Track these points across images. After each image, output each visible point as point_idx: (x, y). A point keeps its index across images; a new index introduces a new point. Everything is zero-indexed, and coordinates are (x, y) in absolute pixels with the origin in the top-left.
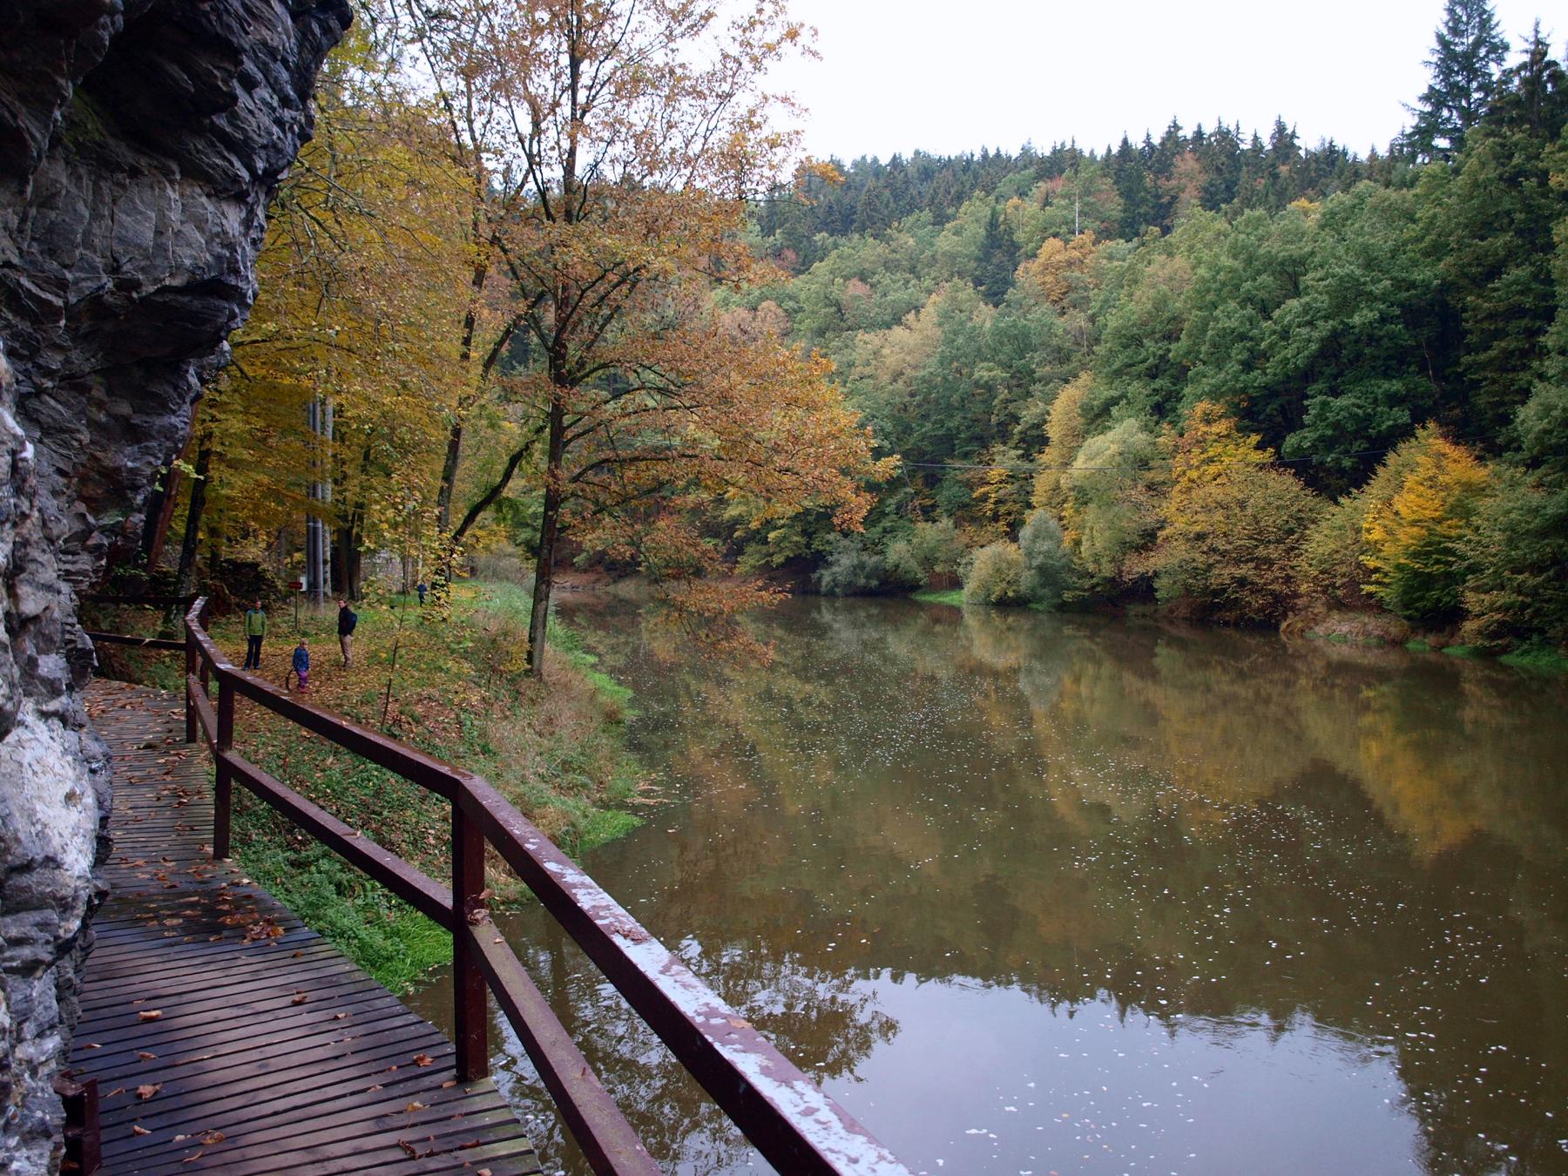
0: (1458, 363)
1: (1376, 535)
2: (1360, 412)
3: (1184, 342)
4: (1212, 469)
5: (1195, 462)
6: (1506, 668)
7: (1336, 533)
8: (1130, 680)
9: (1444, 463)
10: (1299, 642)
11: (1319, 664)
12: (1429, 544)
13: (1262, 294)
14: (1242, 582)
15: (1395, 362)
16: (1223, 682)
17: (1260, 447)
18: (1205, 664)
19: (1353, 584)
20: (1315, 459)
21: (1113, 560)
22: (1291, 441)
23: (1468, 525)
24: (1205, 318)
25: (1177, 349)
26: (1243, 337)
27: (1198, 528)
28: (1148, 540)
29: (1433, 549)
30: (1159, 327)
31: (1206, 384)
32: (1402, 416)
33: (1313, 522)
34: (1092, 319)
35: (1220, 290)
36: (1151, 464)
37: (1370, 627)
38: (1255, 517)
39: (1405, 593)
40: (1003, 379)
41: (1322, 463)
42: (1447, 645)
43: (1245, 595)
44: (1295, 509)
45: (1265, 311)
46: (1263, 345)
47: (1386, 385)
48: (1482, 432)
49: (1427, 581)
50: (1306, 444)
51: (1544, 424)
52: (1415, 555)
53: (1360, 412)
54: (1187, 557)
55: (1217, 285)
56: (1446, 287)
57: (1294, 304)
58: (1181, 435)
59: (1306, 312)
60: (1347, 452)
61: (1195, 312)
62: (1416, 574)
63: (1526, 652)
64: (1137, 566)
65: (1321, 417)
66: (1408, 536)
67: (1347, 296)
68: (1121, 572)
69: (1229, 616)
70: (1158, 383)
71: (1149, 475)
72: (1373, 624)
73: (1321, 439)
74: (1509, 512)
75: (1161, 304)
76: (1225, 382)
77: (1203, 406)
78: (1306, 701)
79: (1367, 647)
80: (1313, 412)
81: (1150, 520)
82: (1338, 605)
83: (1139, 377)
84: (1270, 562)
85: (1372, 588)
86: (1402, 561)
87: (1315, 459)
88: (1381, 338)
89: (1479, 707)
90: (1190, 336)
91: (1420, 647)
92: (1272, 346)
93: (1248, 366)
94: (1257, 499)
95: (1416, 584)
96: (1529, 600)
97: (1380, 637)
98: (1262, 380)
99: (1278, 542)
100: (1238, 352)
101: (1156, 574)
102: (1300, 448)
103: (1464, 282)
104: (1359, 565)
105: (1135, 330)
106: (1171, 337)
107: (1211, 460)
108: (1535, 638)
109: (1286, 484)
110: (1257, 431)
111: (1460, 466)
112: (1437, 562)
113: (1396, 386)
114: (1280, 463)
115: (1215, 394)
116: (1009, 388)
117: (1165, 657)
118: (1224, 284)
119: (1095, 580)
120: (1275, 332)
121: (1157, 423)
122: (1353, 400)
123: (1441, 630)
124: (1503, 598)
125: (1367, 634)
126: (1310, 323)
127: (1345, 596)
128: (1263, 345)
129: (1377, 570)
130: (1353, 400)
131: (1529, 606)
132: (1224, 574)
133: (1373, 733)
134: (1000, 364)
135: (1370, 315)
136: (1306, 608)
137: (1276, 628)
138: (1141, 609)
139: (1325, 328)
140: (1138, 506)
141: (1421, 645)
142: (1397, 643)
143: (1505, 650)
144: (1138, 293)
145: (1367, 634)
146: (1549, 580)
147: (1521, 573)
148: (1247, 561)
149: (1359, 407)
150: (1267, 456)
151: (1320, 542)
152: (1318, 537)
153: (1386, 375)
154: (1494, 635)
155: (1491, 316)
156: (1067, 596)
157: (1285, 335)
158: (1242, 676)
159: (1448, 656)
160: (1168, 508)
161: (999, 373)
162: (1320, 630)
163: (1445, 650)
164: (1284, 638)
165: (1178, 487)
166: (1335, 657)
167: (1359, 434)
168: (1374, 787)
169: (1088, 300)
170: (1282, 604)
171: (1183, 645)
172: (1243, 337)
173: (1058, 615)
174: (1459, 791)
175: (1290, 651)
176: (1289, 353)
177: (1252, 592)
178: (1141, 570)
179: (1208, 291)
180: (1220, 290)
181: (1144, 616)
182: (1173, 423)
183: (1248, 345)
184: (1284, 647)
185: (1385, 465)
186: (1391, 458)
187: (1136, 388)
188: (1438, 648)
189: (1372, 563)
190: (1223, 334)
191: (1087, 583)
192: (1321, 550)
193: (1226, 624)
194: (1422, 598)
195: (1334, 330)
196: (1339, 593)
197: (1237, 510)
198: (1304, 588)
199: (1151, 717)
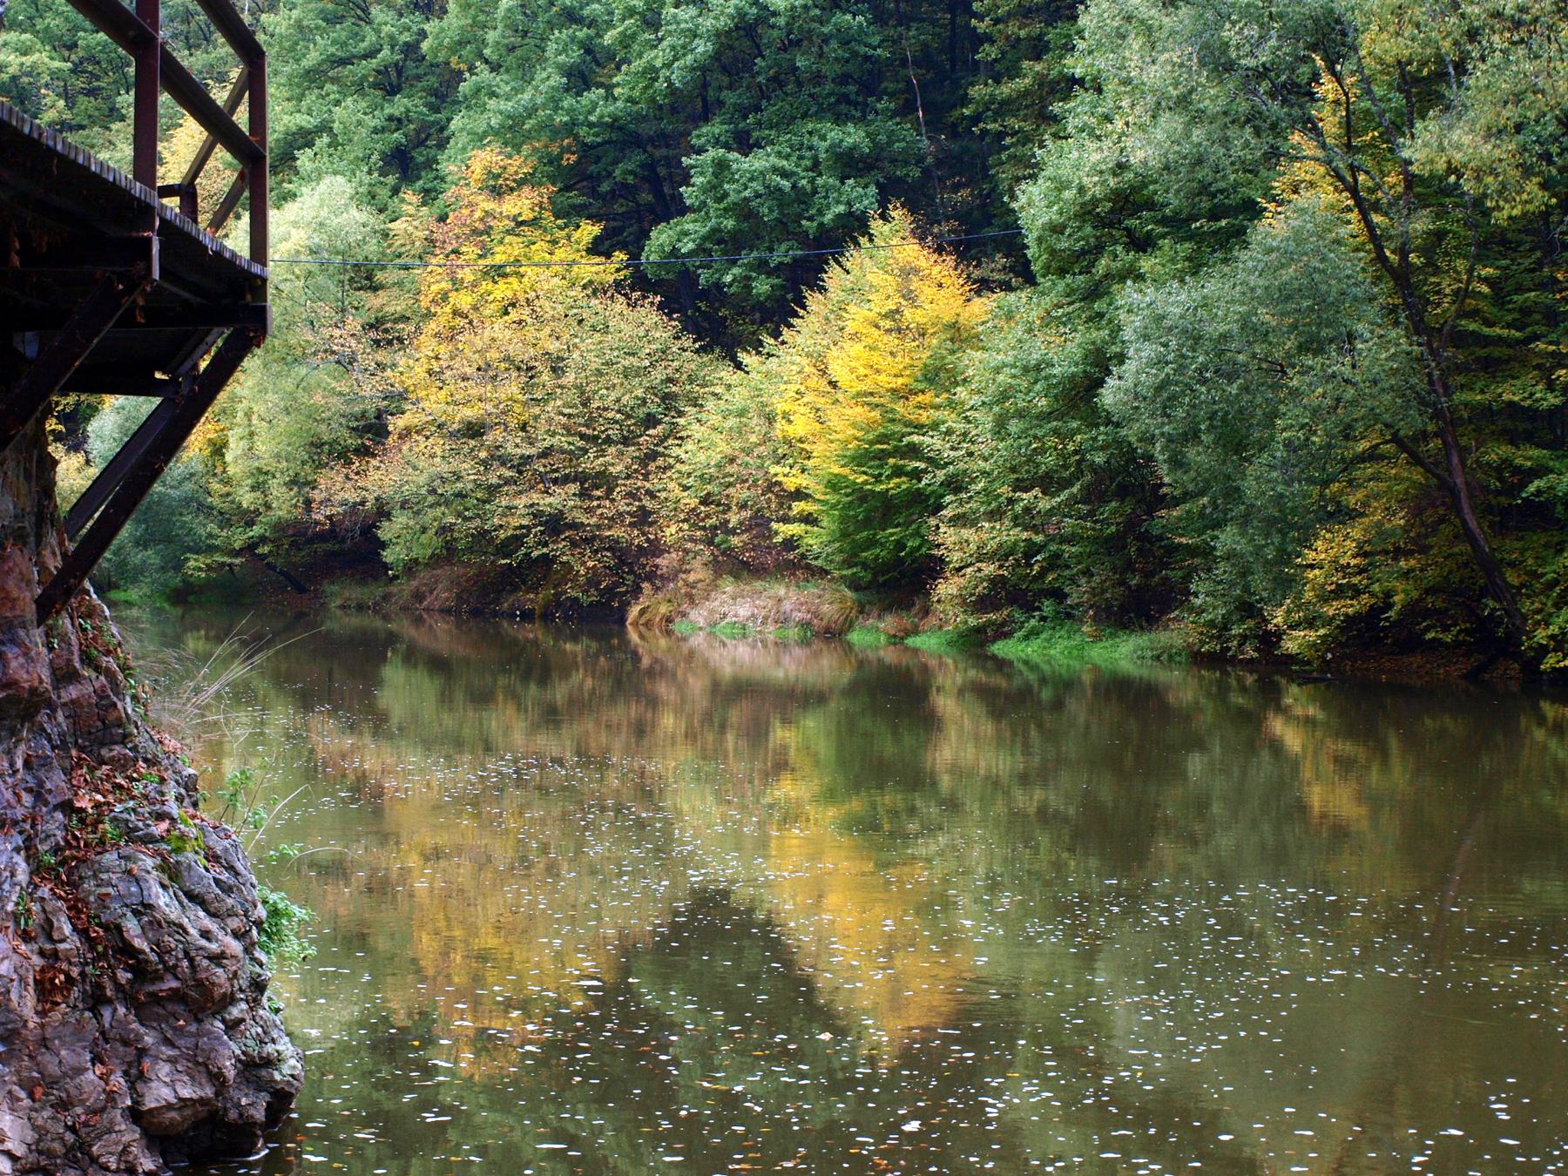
0: (965, 101)
1: (801, 426)
2: (786, 184)
4: (502, 290)
5: (467, 275)
6: (1001, 664)
7: (732, 422)
8: (328, 735)
9: (915, 284)
11: (697, 685)
12: (884, 438)
14: (554, 524)
15: (855, 91)
17: (598, 248)
18: (482, 698)
19: (759, 524)
21: (293, 482)
22: (661, 237)
23: (952, 405)
27: (469, 413)
28: (371, 433)
29: (887, 449)
31: (496, 111)
32: (861, 194)
37: (787, 606)
39: (844, 535)
40: (55, 75)
41: (718, 286)
42: (915, 631)
44: (658, 375)
46: (609, 38)
47: (834, 134)
48: (981, 239)
49: (883, 510)
50: (687, 246)
51: (1052, 215)
53: (786, 184)
54: (444, 468)
58: (442, 219)
60: (762, 266)
62: (862, 496)
63: (1034, 633)
64: (338, 491)
65: (714, 190)
68: (308, 503)
69: (534, 600)
70: (399, 105)
72: (793, 597)
73: (715, 236)
76: (532, 111)
77: (486, 158)
78: (672, 762)
79: (782, 645)
80: (698, 180)
81: (370, 391)
83: (359, 88)
84: (604, 480)
85: (795, 529)
87: (704, 277)
88: (826, 39)
92: (626, 41)
93: (579, 79)
94: (586, 352)
96: (1039, 539)
97: (805, 625)
98: (604, 111)
99: (626, 441)
100: (561, 48)
102: (674, 252)
104: (772, 485)
107: (498, 272)
108: (1048, 606)
109: (644, 325)
110: (594, 218)
111: (941, 291)
112: (898, 472)
113: (853, 136)
114: (638, 283)
115: (512, 133)
116: (69, 97)
117: (401, 688)
119: (257, 530)
121: (395, 191)
122: (774, 160)
123: (908, 607)
124: (1006, 534)
125: (783, 621)
127: (744, 549)
128: (609, 38)
129: (799, 495)
130: (774, 160)
132: (516, 509)
134: (48, 38)
137: (622, 620)
138: (355, 593)
140: (347, 363)
141: (872, 637)
142: (833, 634)
145: (783, 621)
147: (1026, 490)
149: (785, 174)
150: (608, 270)
151: (703, 443)
152: (697, 431)
153: (840, 119)
156: (196, 564)
158: (551, 717)
159: (916, 651)
160: (409, 368)
161: (44, 59)
162: (698, 616)
163: (910, 641)
164: (634, 636)
165: (432, 326)
166: (727, 671)
167: (786, 228)
168: (798, 928)
170: (632, 567)
171: (439, 665)
174: (934, 906)
175: (646, 662)
176: (658, 57)
177: (574, 544)
181: (361, 608)
183: (582, 33)
184: (636, 657)
185: (822, 290)
186: (834, 277)
187: (350, 112)
188: (897, 639)
191: (239, 538)
193: (527, 616)
194: (871, 543)
196: (735, 541)
197: (546, 377)
198: (671, 532)
199: (368, 803)
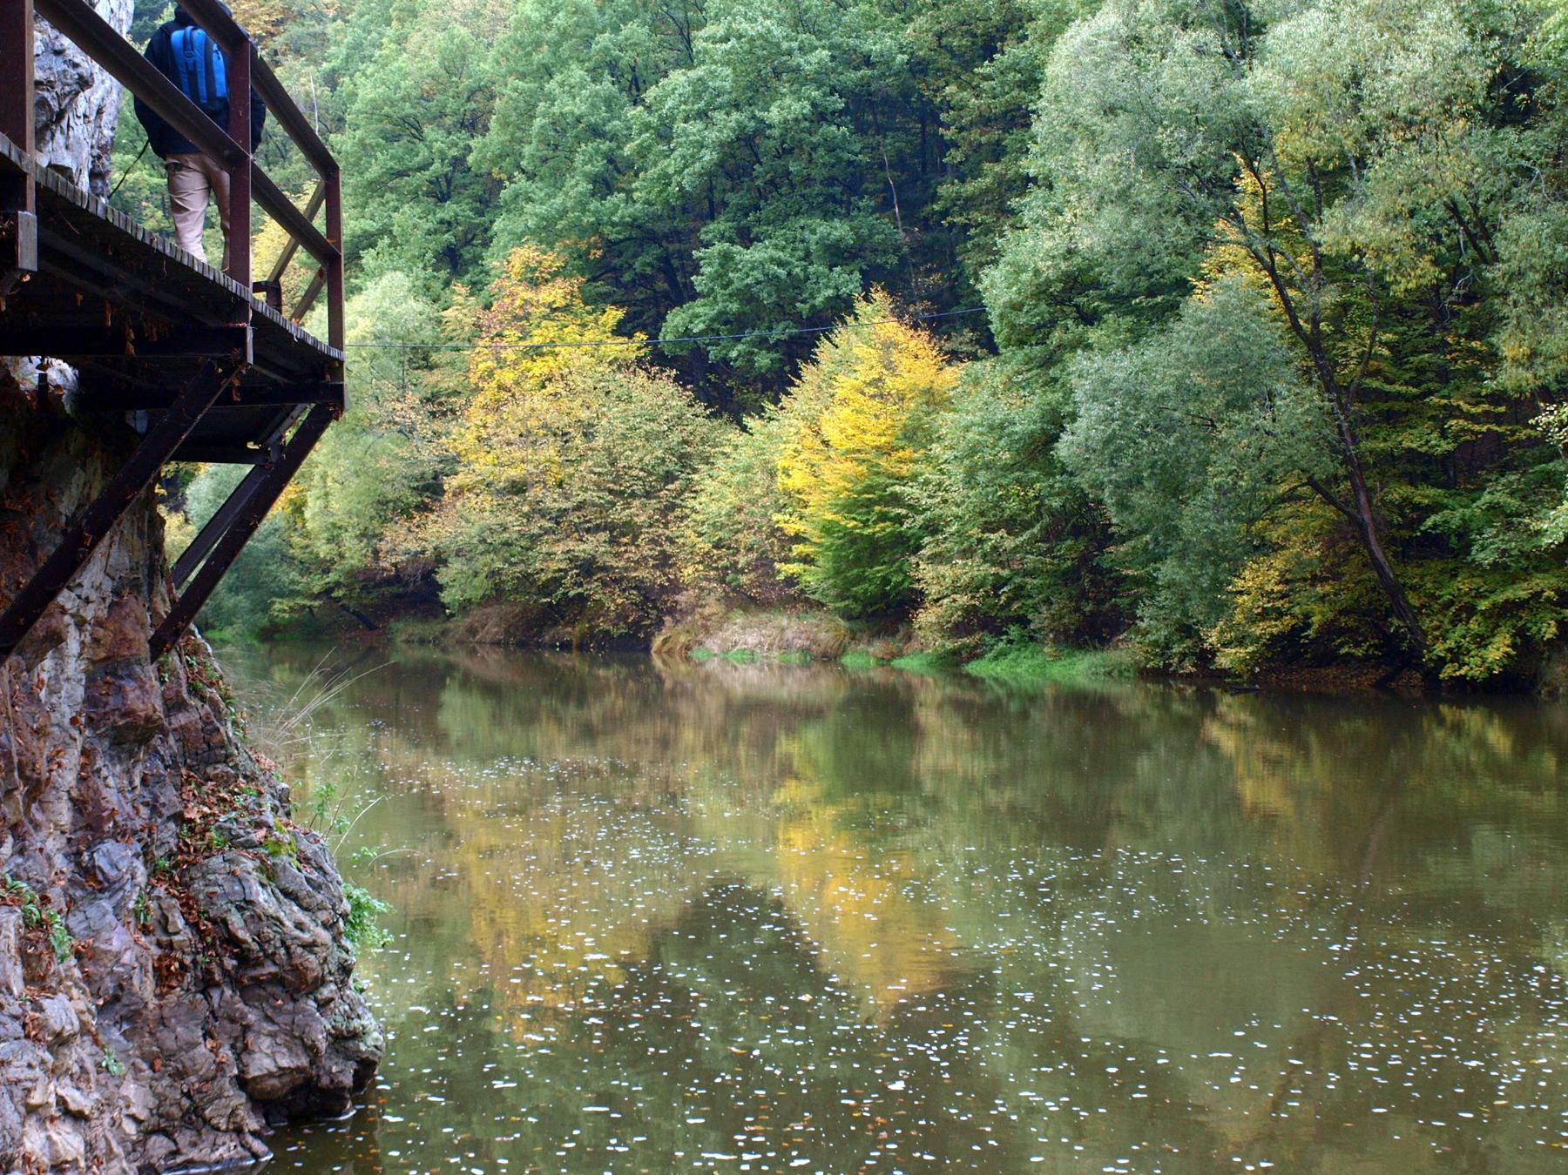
0: (935, 198)
1: (798, 480)
2: (782, 272)
3: (495, 136)
4: (539, 368)
5: (509, 355)
6: (975, 682)
7: (739, 477)
8: (395, 753)
9: (895, 356)
10: (683, 668)
11: (713, 704)
12: (869, 489)
13: (627, 58)
14: (588, 568)
15: (843, 189)
16: (560, 750)
17: (622, 330)
19: (764, 564)
20: (713, 353)
22: (676, 319)
23: (928, 459)
24: (532, 94)
25: (482, 149)
26: (596, 132)
27: (514, 473)
29: (874, 498)
30: (452, 105)
31: (532, 214)
32: (846, 280)
33: (706, 460)
34: (331, 80)
35: (558, 44)
36: (434, 357)
37: (789, 634)
38: (609, 451)
42: (900, 654)
43: (593, 588)
44: (675, 438)
45: (635, 86)
46: (628, 150)
47: (823, 228)
50: (698, 327)
52: (849, 507)
53: (782, 272)
54: (492, 521)
55: (551, 35)
56: (918, 67)
57: (678, 77)
58: (488, 307)
59: (698, 95)
60: (762, 343)
61: (513, 82)
62: (852, 539)
63: (1003, 654)
64: (403, 542)
65: (721, 277)
66: (839, 475)
67: (764, 72)
69: (571, 633)
70: (449, 210)
71: (430, 378)
72: (792, 626)
73: (723, 318)
74: (967, 429)
75: (455, 63)
76: (563, 213)
77: (524, 254)
79: (785, 668)
80: (707, 270)
81: (428, 455)
82: (748, 602)
83: (415, 197)
86: (829, 516)
87: (713, 353)
89: (943, 749)
90: (505, 124)
91: (861, 661)
92: (643, 152)
93: (603, 185)
94: (613, 419)
95: (860, 552)
96: (1005, 573)
97: (805, 650)
98: (625, 212)
100: (587, 159)
101: (440, 559)
103: (944, 60)
104: (774, 531)
105: (408, 109)
106: (473, 124)
107: (536, 352)
108: (1014, 631)
109: (662, 395)
111: (917, 361)
112: (883, 517)
113: (839, 230)
114: (658, 359)
115: (546, 232)
117: (458, 710)
118: (564, 34)
119: (332, 577)
120: (647, 127)
121: (447, 284)
122: (772, 252)
123: (894, 633)
124: (976, 569)
125: (786, 647)
126: (702, 115)
128: (628, 150)
129: (798, 538)
130: (772, 252)
131: (1007, 581)
132: (554, 556)
133: (797, 816)
135: (796, 106)
136: (691, 610)
137: (647, 649)
138: (418, 629)
139: (727, 124)
140: (407, 432)
141: (863, 659)
142: (829, 658)
143: (974, 654)
144: (415, 38)
145: (786, 647)
146: (1034, 540)
147: (993, 531)
148: (597, 529)
149: (781, 264)
150: (631, 348)
151: (714, 496)
153: (827, 216)
154: (958, 629)
155: (985, 121)
156: (280, 606)
157: (664, 133)
158: (588, 733)
159: (901, 671)
160: (461, 436)
162: (713, 644)
163: (897, 663)
165: (480, 399)
166: (739, 691)
167: (783, 310)
169: (323, 40)
170: (655, 603)
171: (491, 690)
172: (596, 132)
173: (264, 648)
175: (668, 684)
177: (605, 584)
178: (414, 546)
179: (537, 44)
180: (558, 44)
182: (476, 287)
185: (815, 362)
186: (824, 351)
188: (884, 661)
189: (792, 528)
190: (558, 124)
192: (714, 507)
193: (566, 646)
194: (861, 579)
195: (741, 127)
196: (743, 579)
197: (578, 441)
199: (430, 811)
